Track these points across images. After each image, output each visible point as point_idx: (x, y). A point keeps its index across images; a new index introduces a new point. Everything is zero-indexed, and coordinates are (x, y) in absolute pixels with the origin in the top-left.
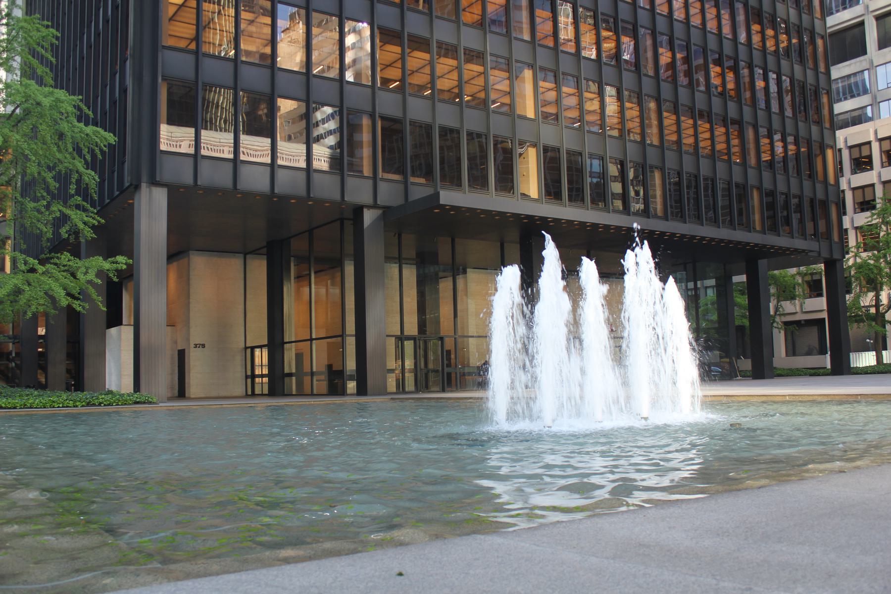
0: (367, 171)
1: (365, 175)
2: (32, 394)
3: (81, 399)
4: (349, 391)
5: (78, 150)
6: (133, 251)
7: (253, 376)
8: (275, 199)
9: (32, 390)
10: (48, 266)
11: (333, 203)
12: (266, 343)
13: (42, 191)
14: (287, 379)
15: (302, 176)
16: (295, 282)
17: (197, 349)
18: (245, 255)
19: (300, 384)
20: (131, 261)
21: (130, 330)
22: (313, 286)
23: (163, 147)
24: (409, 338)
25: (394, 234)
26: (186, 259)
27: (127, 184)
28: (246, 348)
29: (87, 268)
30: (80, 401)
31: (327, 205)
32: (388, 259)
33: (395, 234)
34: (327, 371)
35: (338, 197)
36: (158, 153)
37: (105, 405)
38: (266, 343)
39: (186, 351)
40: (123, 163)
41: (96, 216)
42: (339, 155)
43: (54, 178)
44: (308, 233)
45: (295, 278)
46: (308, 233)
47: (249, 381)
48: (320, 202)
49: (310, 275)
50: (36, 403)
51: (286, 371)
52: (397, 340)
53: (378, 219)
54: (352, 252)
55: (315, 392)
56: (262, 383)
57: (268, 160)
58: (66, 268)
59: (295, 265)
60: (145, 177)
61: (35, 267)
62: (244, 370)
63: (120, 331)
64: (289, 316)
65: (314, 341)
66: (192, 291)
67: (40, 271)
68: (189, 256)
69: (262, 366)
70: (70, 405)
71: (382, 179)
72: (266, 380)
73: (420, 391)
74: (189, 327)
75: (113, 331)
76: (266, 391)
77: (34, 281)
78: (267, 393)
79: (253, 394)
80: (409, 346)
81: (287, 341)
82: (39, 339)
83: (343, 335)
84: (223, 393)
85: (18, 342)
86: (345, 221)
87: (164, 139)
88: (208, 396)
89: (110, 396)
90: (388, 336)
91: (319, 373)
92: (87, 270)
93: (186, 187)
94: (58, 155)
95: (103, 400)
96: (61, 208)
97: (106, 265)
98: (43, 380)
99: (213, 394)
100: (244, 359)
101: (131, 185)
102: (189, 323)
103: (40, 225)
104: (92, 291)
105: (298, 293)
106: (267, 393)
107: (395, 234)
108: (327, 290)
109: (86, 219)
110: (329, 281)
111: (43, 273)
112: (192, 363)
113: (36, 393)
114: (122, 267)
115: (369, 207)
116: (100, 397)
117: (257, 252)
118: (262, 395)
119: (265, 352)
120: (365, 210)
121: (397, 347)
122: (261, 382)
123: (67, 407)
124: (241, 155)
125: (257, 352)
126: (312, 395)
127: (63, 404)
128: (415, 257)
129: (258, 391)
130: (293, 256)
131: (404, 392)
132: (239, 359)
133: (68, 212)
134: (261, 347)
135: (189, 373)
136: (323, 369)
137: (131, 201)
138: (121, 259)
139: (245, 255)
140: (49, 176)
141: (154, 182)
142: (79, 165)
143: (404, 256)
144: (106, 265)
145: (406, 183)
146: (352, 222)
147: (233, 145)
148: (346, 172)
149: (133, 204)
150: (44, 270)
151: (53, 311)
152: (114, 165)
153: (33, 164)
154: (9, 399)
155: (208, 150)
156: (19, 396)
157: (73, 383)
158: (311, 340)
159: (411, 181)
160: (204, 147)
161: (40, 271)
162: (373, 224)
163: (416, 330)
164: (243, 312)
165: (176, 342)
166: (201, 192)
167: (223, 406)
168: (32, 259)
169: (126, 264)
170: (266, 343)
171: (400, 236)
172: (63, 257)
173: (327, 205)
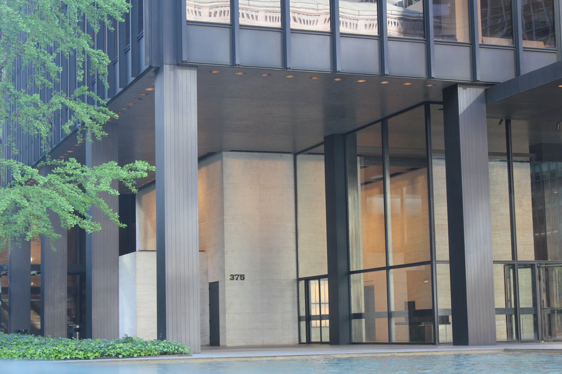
0: (461, 35)
1: (459, 41)
2: (31, 342)
3: (93, 349)
4: (442, 339)
5: (84, 25)
6: (154, 154)
7: (309, 318)
8: (337, 80)
9: (31, 337)
10: (50, 176)
11: (414, 80)
12: (326, 273)
13: (42, 78)
14: (354, 322)
15: (374, 45)
16: (362, 190)
17: (235, 281)
18: (295, 155)
19: (370, 328)
20: (153, 168)
21: (152, 258)
22: (388, 195)
23: (190, 17)
24: (525, 265)
25: (499, 120)
26: (218, 163)
27: (144, 67)
28: (299, 280)
29: (99, 178)
30: (92, 352)
31: (407, 84)
32: (493, 155)
33: (502, 120)
34: (407, 311)
35: (421, 73)
36: (184, 24)
37: (124, 357)
38: (326, 273)
39: (220, 284)
40: (139, 39)
41: (107, 109)
42: (422, 15)
43: (55, 61)
44: (380, 123)
45: (362, 184)
46: (380, 123)
47: (303, 324)
48: (399, 80)
49: (384, 179)
50: (38, 353)
51: (354, 310)
52: (507, 267)
53: (478, 100)
54: (443, 148)
55: (394, 340)
56: (321, 327)
57: (227, 20)
58: (72, 178)
59: (361, 167)
60: (168, 57)
61: (33, 178)
62: (296, 310)
63: (135, 257)
64: (357, 235)
65: (391, 270)
66: (226, 204)
67: (41, 183)
68: (222, 157)
69: (320, 303)
70: (80, 357)
71: (483, 46)
72: (326, 323)
73: (542, 339)
74: (223, 253)
75: (126, 259)
76: (326, 337)
77: (34, 197)
78: (328, 340)
79: (309, 342)
80: (524, 275)
81: (355, 270)
82: (31, 270)
83: (431, 262)
84: (268, 341)
85: (6, 274)
86: (432, 106)
87: (191, 5)
88: (250, 343)
89: (130, 345)
90: (495, 262)
91: (399, 314)
92: (98, 180)
93: (220, 67)
94: (61, 33)
95: (122, 350)
96: (63, 100)
97: (123, 173)
98: (38, 325)
99: (257, 341)
100: (296, 295)
101: (150, 67)
102: (223, 247)
103: (37, 124)
104: (104, 206)
105: (366, 207)
106: (328, 340)
107: (502, 120)
108: (402, 200)
109: (94, 113)
110: (404, 189)
111: (45, 186)
112: (228, 300)
113: (36, 340)
114: (142, 175)
115: (465, 85)
116: (118, 346)
117: (311, 151)
118: (321, 343)
119: (325, 284)
120: (460, 90)
121: (506, 277)
122: (319, 325)
123: (76, 358)
124: (292, 22)
125: (314, 285)
126: (390, 343)
127: (71, 355)
128: (528, 152)
129: (315, 337)
130: (358, 155)
131: (519, 340)
132: (289, 296)
133: (70, 104)
134: (319, 278)
135: (225, 313)
136: (403, 308)
137: (150, 89)
138: (141, 165)
139: (295, 155)
140: (49, 59)
141: (180, 63)
142: (85, 43)
143: (514, 150)
144: (123, 173)
145: (516, 49)
146: (441, 106)
147: (280, 9)
148: (432, 39)
149: (153, 92)
150: (46, 181)
151: (55, 235)
152: (128, 42)
153: (32, 44)
154: (4, 348)
155: (249, 18)
156: (17, 345)
157: (78, 327)
158: (388, 268)
159: (524, 46)
160: (243, 14)
161: (41, 183)
162: (470, 109)
163: (532, 253)
164: (294, 231)
165: (206, 273)
166: (239, 74)
167: (277, 358)
168: (30, 168)
169: (147, 171)
170: (326, 273)
171: (508, 122)
172: (68, 164)
173: (407, 84)
